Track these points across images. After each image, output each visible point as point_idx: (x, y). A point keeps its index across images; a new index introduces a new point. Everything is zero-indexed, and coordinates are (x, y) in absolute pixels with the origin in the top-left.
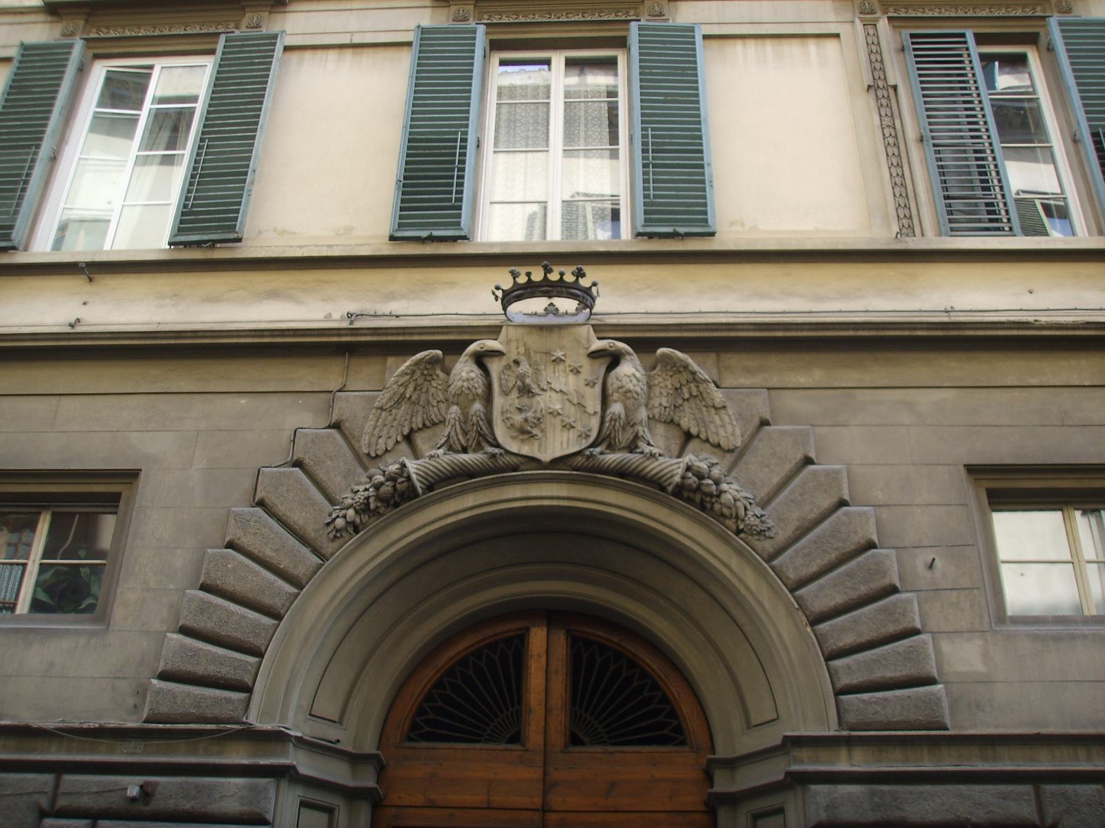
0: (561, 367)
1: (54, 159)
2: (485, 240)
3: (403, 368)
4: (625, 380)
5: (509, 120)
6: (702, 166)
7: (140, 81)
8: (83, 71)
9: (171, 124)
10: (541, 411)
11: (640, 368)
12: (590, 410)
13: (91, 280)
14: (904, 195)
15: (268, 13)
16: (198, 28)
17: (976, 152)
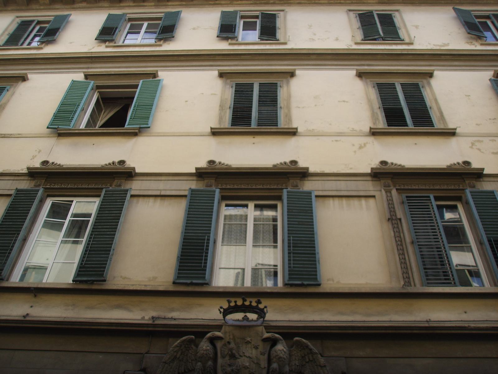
0: (249, 345)
1: (25, 240)
2: (216, 285)
3: (176, 344)
4: (279, 352)
5: (229, 231)
6: (315, 254)
7: (67, 207)
8: (42, 202)
9: (78, 227)
10: (240, 366)
11: (286, 347)
12: (262, 366)
13: (35, 296)
14: (406, 267)
15: (124, 180)
16: (94, 185)
17: (437, 248)
